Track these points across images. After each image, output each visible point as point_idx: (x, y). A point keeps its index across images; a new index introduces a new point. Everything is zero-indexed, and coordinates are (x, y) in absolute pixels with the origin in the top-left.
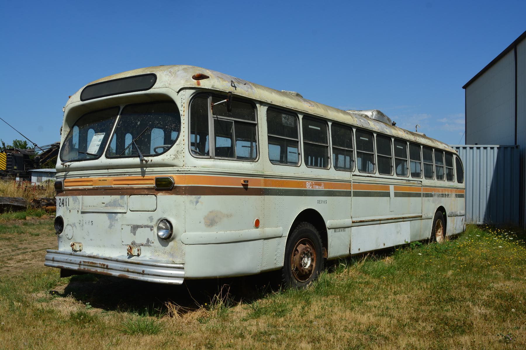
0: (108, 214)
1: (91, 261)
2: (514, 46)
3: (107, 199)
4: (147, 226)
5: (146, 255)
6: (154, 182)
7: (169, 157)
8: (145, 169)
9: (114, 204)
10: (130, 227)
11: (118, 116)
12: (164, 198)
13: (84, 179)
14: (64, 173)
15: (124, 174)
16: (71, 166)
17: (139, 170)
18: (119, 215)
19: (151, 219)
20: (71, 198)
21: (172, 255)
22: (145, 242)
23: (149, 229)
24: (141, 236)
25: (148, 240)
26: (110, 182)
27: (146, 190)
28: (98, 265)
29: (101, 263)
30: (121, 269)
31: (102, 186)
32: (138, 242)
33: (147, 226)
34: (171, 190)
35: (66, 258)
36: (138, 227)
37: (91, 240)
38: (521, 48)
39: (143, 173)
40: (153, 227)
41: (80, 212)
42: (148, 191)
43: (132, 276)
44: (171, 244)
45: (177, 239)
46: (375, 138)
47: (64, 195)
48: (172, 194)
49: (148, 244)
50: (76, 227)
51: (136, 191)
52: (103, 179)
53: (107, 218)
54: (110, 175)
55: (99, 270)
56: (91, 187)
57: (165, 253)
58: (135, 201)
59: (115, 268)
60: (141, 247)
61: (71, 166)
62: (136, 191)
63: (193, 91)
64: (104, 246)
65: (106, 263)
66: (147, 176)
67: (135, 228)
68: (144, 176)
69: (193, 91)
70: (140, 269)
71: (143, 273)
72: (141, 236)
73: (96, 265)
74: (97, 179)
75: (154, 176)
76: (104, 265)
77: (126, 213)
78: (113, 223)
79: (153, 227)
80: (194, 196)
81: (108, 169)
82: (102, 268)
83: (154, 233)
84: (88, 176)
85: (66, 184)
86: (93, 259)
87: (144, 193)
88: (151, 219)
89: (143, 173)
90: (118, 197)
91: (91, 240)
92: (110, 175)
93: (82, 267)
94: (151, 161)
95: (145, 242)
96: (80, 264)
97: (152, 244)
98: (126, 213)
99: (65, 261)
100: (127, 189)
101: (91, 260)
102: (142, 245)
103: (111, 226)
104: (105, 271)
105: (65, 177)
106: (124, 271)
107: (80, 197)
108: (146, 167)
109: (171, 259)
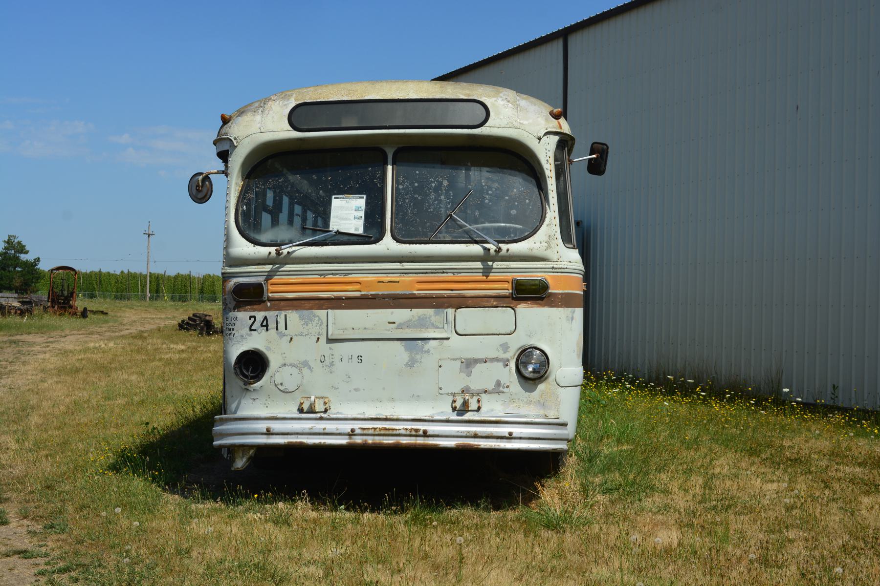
0: (404, 342)
1: (380, 426)
2: (564, 34)
3: (401, 315)
4: (497, 360)
5: (492, 408)
6: (509, 286)
7: (538, 245)
8: (490, 263)
9: (422, 324)
10: (458, 364)
11: (390, 168)
12: (527, 312)
13: (330, 278)
14: (268, 268)
15: (443, 271)
16: (294, 255)
17: (479, 265)
18: (432, 342)
19: (505, 347)
20: (293, 316)
21: (543, 406)
22: (491, 386)
23: (501, 364)
24: (482, 377)
25: (498, 384)
26: (407, 283)
27: (492, 300)
28: (403, 432)
29: (409, 427)
30: (460, 434)
31: (386, 293)
32: (475, 386)
33: (497, 360)
34: (542, 299)
35: (310, 426)
36: (476, 361)
37: (356, 390)
38: (575, 41)
39: (487, 271)
40: (508, 360)
41: (323, 339)
42: (498, 301)
43: (484, 444)
44: (541, 387)
45: (551, 379)
46: (508, 225)
47: (267, 309)
48: (544, 306)
49: (498, 389)
50: (310, 368)
51: (470, 302)
52: (389, 279)
53: (403, 349)
54: (406, 272)
55: (405, 441)
56: (357, 294)
57: (530, 403)
58: (467, 317)
59: (444, 434)
60: (483, 395)
61: (294, 255)
62: (470, 302)
63: (557, 138)
64: (393, 400)
65: (422, 427)
66: (492, 276)
67: (469, 364)
68: (487, 276)
69: (557, 138)
70: (504, 430)
71: (510, 437)
72: (482, 377)
73: (398, 432)
74: (369, 279)
75: (510, 276)
76: (417, 430)
77: (448, 339)
78: (418, 357)
79: (508, 360)
80: (570, 309)
81: (401, 262)
82: (411, 436)
83: (510, 369)
84: (346, 273)
85: (271, 288)
86: (384, 422)
87: (489, 304)
88: (505, 347)
89: (487, 271)
90: (430, 312)
91: (356, 390)
92: (406, 272)
93: (358, 440)
94: (508, 250)
95: (491, 386)
96: (352, 434)
97: (505, 390)
98: (448, 339)
99: (322, 431)
100: (449, 297)
101: (379, 425)
102: (485, 392)
103: (411, 364)
104: (420, 441)
105: (269, 276)
106: (466, 437)
107: (322, 313)
108: (494, 261)
109: (542, 412)
